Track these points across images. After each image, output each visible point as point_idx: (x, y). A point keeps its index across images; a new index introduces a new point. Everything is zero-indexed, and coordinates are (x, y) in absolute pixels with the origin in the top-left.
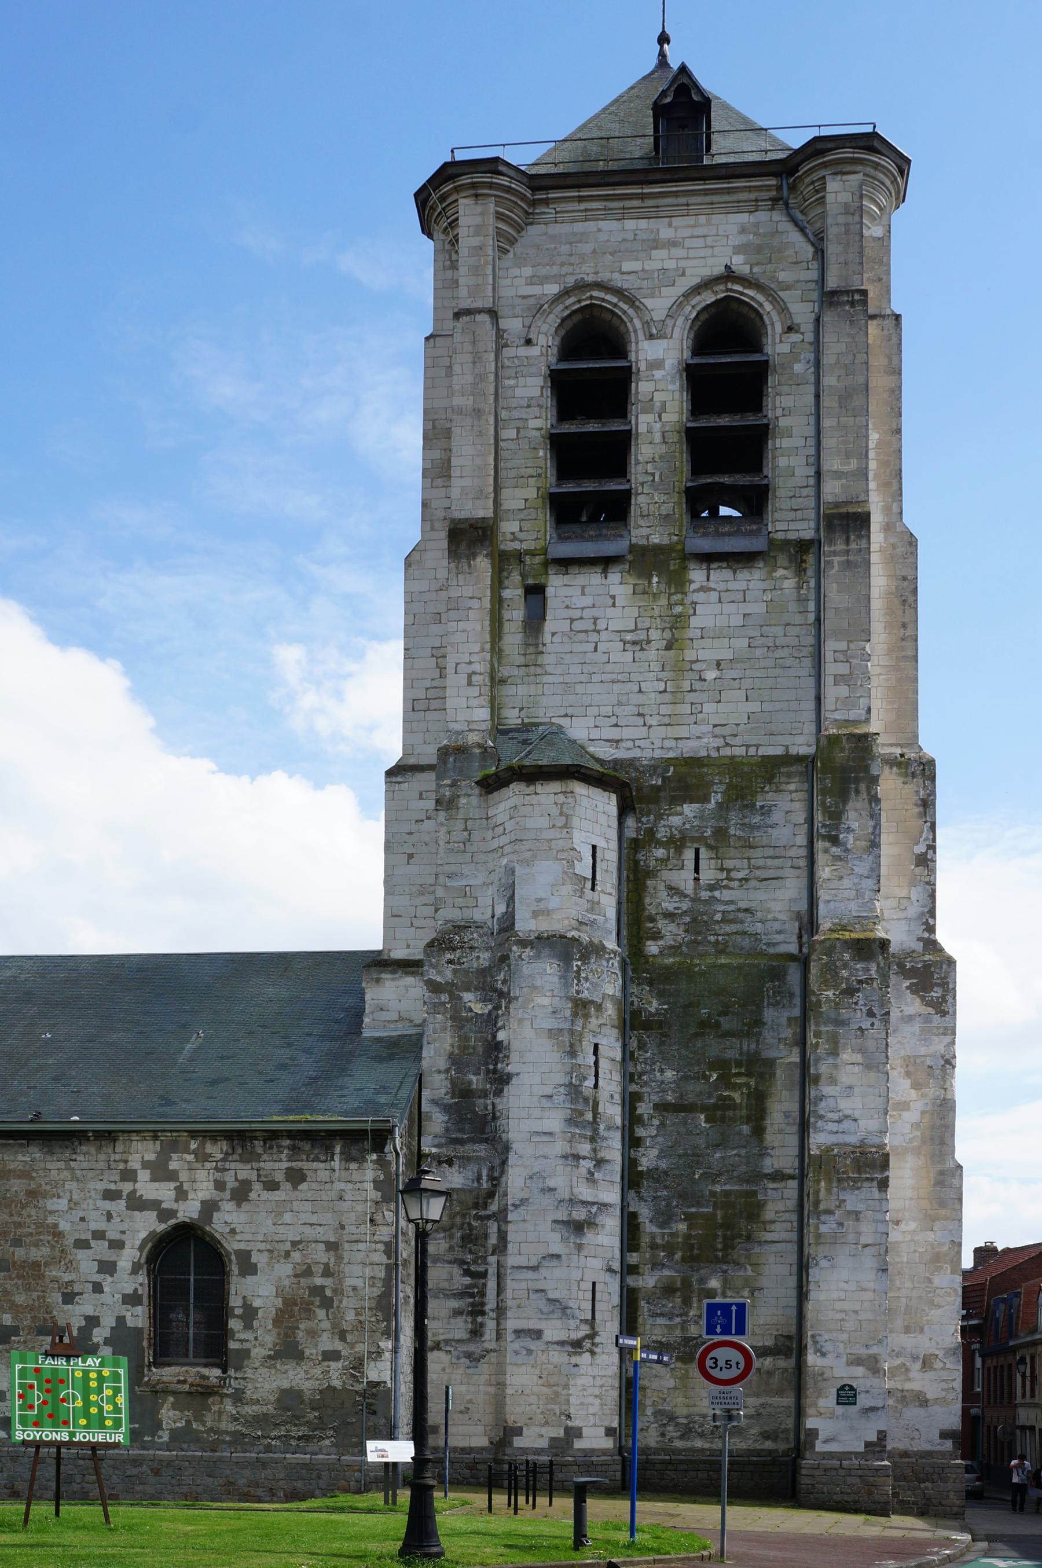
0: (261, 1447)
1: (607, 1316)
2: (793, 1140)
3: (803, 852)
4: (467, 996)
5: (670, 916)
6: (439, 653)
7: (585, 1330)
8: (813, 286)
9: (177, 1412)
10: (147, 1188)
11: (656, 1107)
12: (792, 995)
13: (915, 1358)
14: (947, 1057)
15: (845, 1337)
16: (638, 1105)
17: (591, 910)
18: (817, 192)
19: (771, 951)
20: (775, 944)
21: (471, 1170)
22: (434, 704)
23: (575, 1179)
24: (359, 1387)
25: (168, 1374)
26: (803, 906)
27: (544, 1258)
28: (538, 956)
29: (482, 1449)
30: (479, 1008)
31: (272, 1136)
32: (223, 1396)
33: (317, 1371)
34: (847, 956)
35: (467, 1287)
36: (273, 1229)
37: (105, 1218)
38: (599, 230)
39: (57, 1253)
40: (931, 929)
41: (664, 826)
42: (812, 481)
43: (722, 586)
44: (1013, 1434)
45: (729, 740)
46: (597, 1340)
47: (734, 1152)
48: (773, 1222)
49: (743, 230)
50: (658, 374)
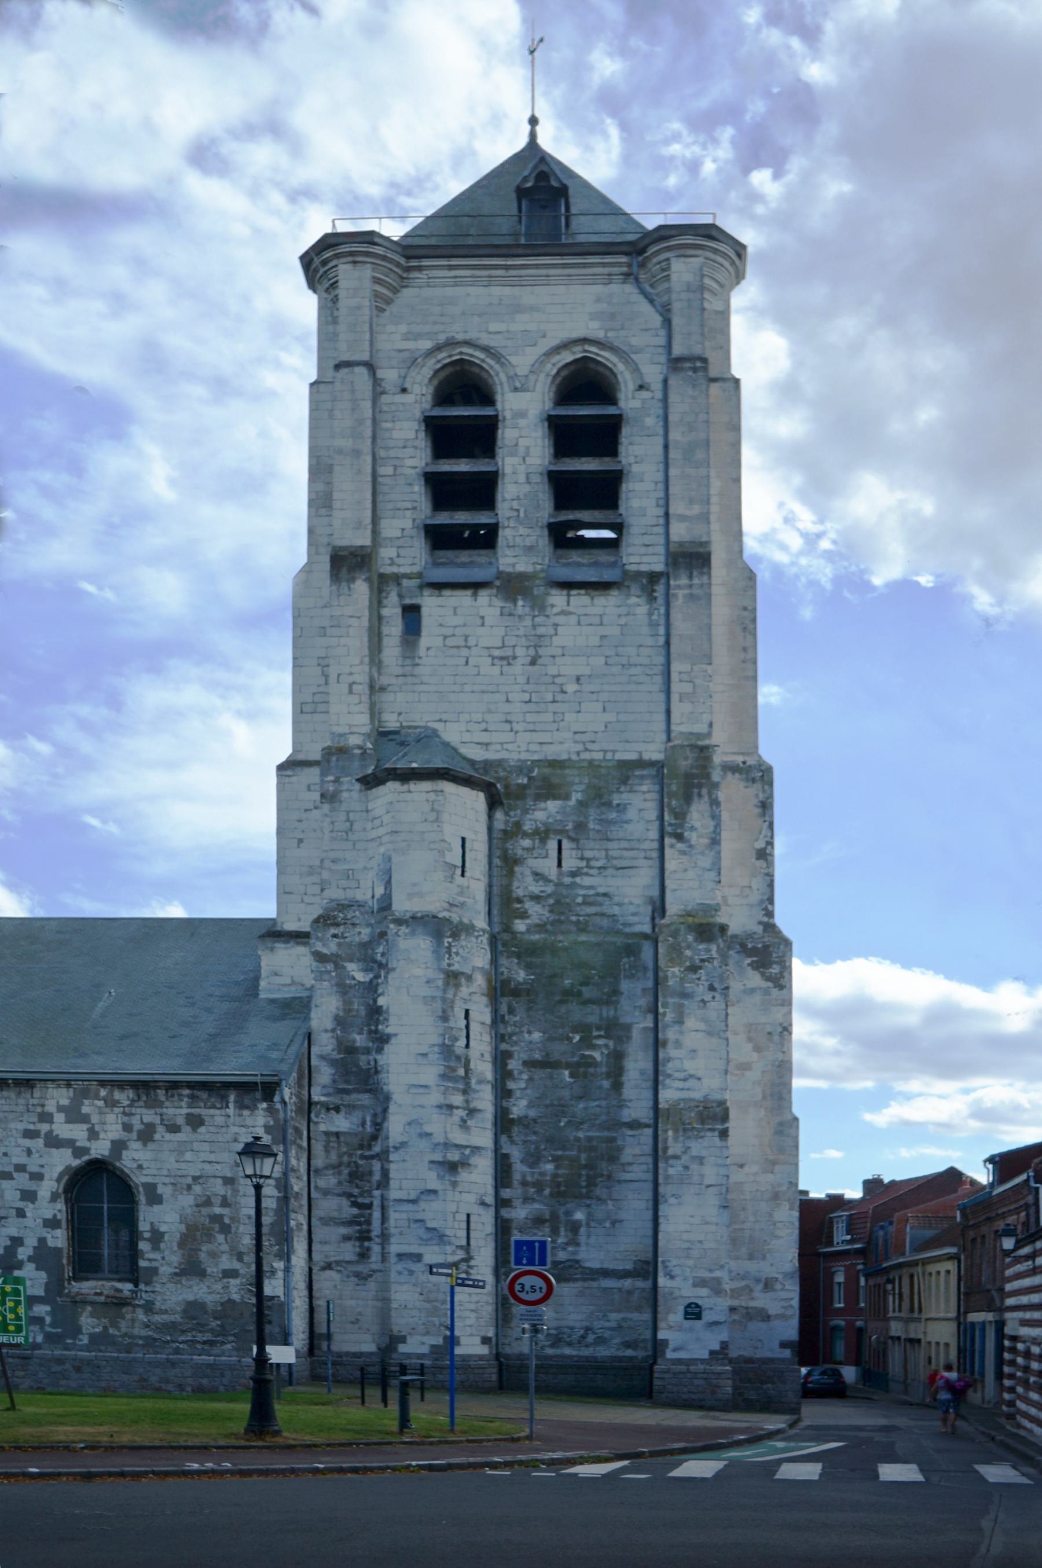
0: (171, 1350)
1: (482, 1243)
2: (648, 1094)
3: (655, 845)
5: (536, 898)
6: (324, 662)
7: (460, 1255)
8: (661, 350)
9: (95, 1320)
10: (63, 1129)
11: (525, 1063)
13: (758, 1281)
14: (785, 1025)
15: (691, 1262)
16: (509, 1061)
17: (461, 894)
18: (663, 270)
19: (627, 930)
20: (630, 925)
21: (356, 1117)
22: (321, 708)
23: (448, 1126)
25: (87, 1287)
26: (655, 892)
27: (422, 1193)
28: (413, 933)
29: (372, 1354)
30: (361, 977)
31: (173, 1086)
33: (218, 1287)
34: (690, 938)
35: (355, 1216)
36: (176, 1165)
37: (25, 1154)
38: (468, 295)
40: (770, 914)
41: (530, 820)
42: (662, 521)
43: (581, 611)
44: (885, 1343)
45: (589, 746)
46: (472, 1263)
47: (596, 1103)
48: (630, 1164)
49: (598, 300)
50: (522, 422)
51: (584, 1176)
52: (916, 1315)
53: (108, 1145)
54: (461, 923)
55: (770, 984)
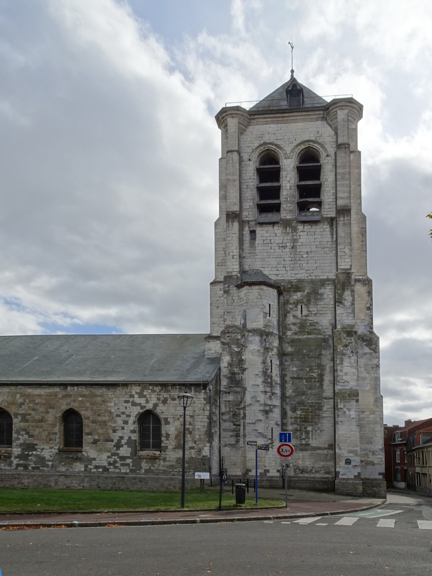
2: (331, 388)
3: (333, 306)
4: (233, 346)
5: (294, 324)
7: (270, 441)
8: (334, 143)
10: (137, 399)
11: (291, 378)
12: (330, 347)
13: (370, 451)
18: (335, 115)
24: (200, 457)
25: (144, 453)
26: (333, 321)
28: (253, 335)
29: (240, 476)
31: (174, 385)
32: (160, 459)
39: (111, 418)
40: (372, 328)
42: (334, 200)
43: (308, 230)
44: (414, 475)
45: (311, 274)
46: (273, 444)
51: (310, 416)
52: (425, 465)
53: (152, 405)
54: (269, 332)
55: (372, 351)
